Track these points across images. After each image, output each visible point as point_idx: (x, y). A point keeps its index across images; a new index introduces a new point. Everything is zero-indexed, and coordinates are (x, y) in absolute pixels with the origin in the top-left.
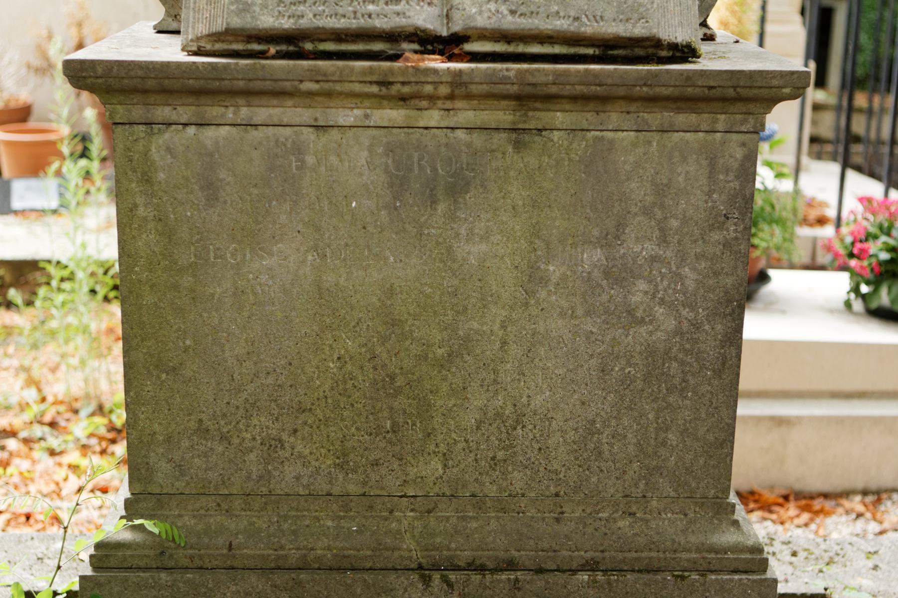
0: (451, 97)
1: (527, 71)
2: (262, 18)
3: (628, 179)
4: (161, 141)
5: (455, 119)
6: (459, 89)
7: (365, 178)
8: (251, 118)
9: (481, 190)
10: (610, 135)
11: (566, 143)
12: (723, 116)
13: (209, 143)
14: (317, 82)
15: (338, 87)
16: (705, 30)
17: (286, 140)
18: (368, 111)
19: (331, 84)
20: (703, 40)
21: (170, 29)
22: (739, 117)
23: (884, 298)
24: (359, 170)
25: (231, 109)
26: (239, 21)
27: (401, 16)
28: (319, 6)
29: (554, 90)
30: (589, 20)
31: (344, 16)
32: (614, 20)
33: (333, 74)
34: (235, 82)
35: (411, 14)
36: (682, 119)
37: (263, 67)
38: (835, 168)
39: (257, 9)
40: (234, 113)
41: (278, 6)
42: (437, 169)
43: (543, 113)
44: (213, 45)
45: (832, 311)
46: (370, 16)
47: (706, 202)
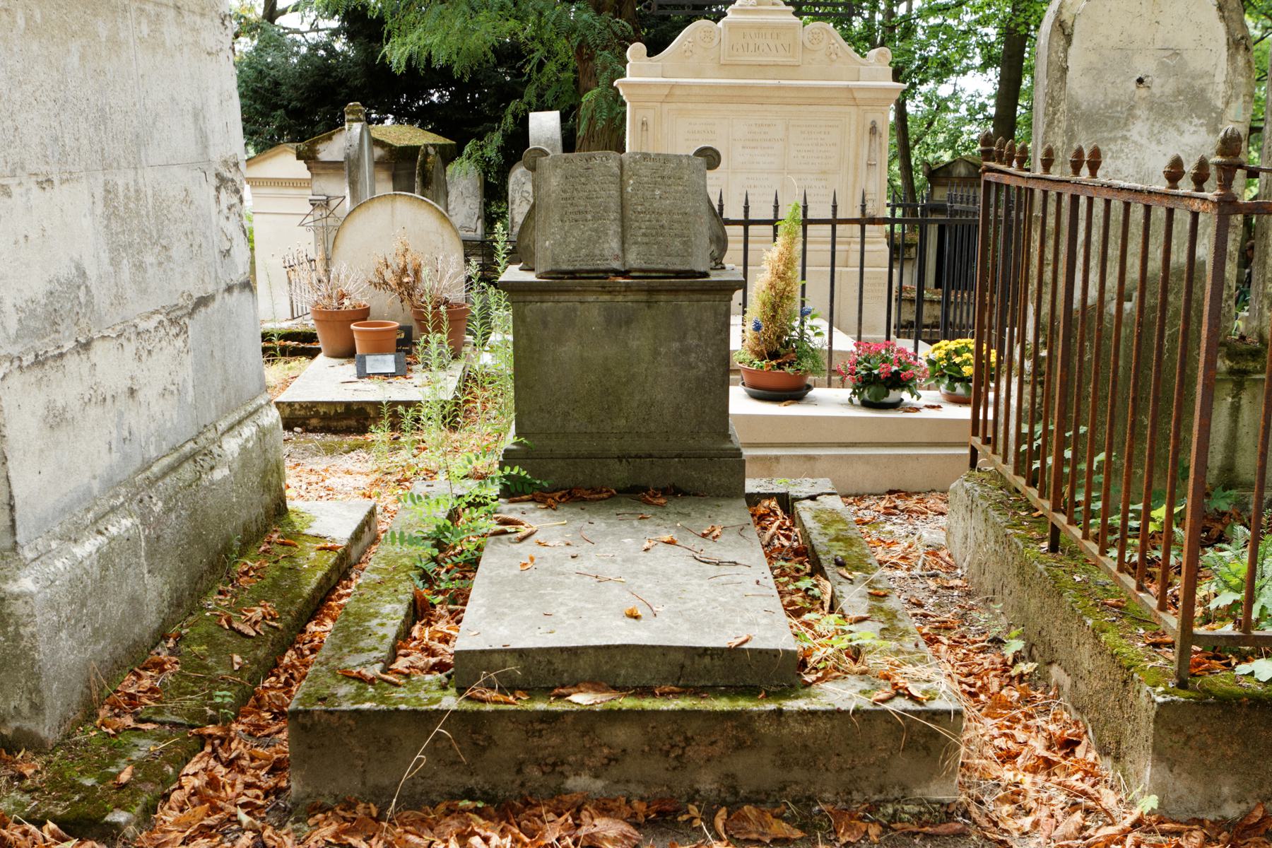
36: (704, 297)
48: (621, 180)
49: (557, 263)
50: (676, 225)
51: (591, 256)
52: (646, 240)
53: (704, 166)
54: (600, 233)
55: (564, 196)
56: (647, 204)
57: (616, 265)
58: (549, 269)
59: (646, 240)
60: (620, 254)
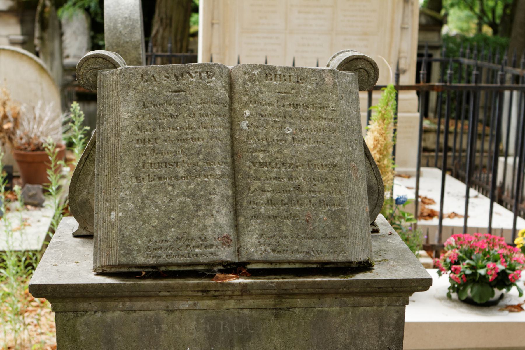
0: (242, 295)
1: (282, 283)
2: (138, 258)
3: (336, 331)
4: (82, 320)
5: (243, 304)
6: (245, 290)
7: (194, 335)
8: (132, 307)
9: (257, 340)
10: (326, 309)
11: (303, 314)
12: (387, 298)
13: (109, 320)
14: (169, 292)
15: (180, 294)
16: (373, 227)
17: (151, 317)
18: (196, 302)
19: (176, 292)
20: (372, 232)
21: (82, 235)
22: (395, 298)
23: (469, 292)
24: (191, 331)
25: (121, 303)
26: (125, 260)
27: (214, 255)
28: (169, 250)
29: (296, 291)
30: (314, 253)
31: (183, 256)
32: (328, 252)
33: (177, 288)
34: (124, 293)
35: (219, 253)
36: (364, 300)
37: (139, 285)
38: (438, 173)
39: (135, 253)
40: (123, 305)
41: (147, 251)
42: (233, 330)
43: (290, 300)
44: (111, 269)
45: (440, 299)
46: (197, 255)
47: (378, 341)
48: (231, 109)
49: (129, 252)
50: (320, 186)
51: (184, 239)
52: (273, 211)
53: (354, 87)
54: (199, 199)
55: (141, 135)
56: (273, 150)
57: (226, 254)
58: (114, 261)
59: (273, 211)
60: (232, 234)
